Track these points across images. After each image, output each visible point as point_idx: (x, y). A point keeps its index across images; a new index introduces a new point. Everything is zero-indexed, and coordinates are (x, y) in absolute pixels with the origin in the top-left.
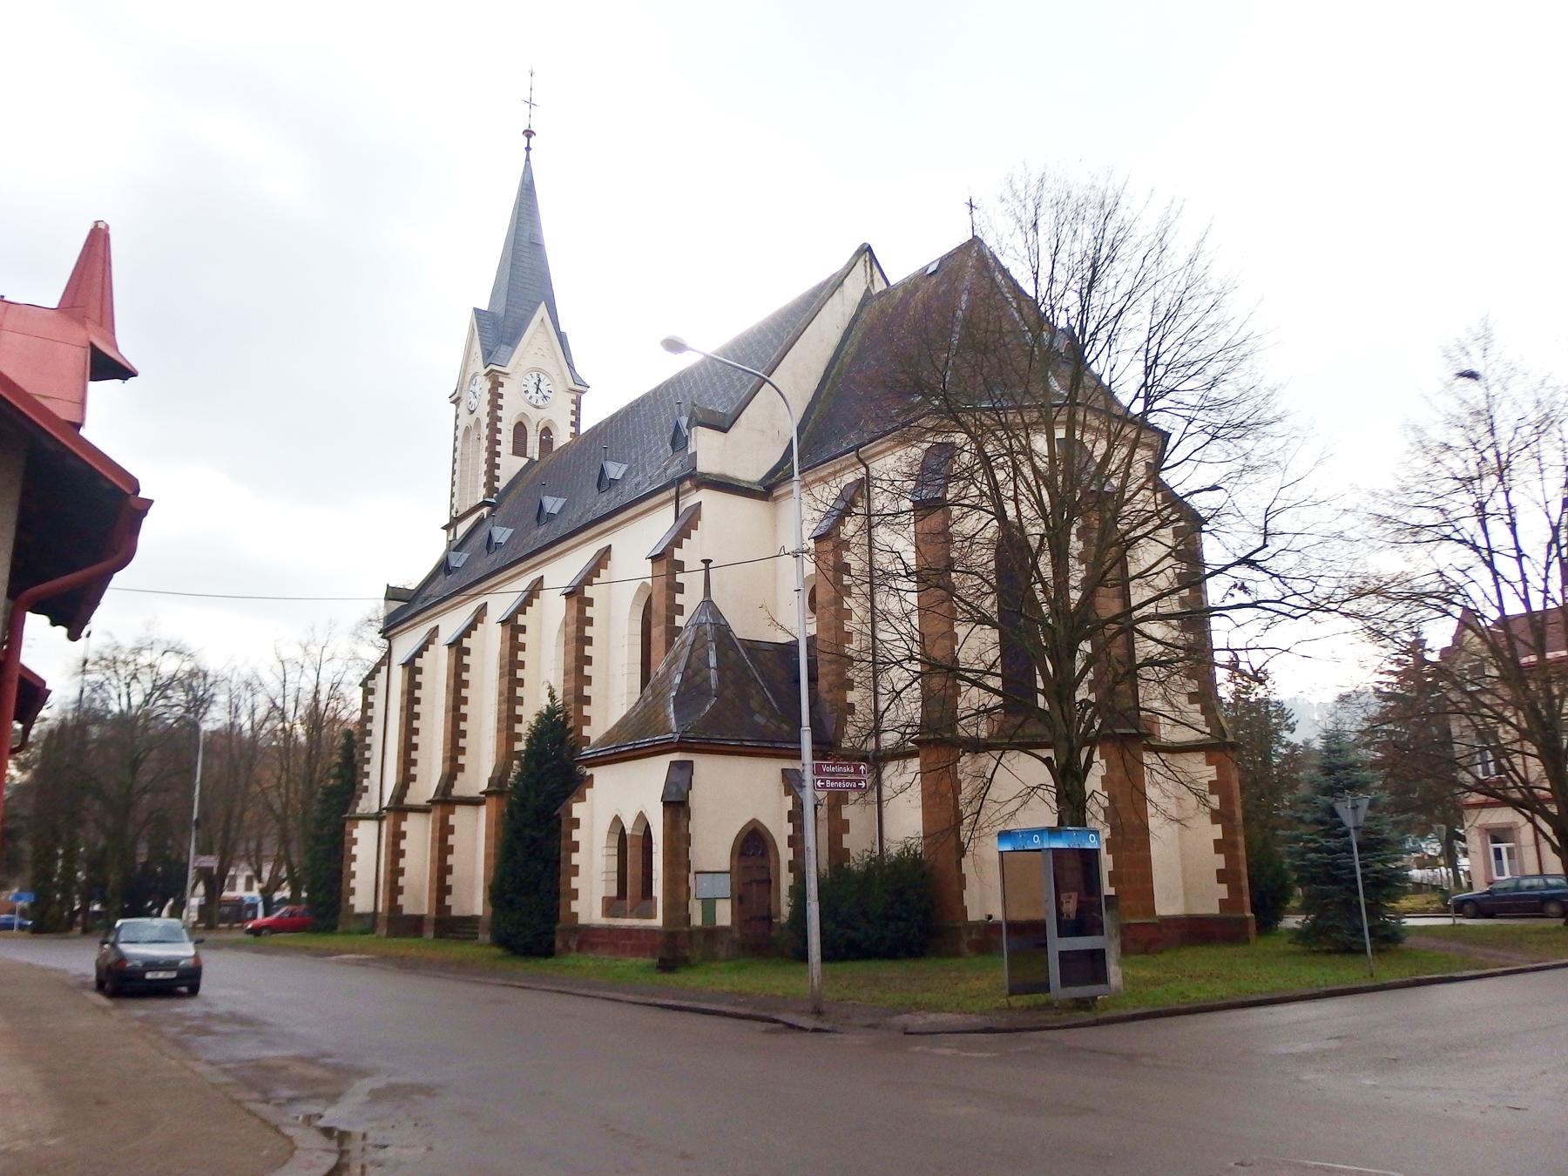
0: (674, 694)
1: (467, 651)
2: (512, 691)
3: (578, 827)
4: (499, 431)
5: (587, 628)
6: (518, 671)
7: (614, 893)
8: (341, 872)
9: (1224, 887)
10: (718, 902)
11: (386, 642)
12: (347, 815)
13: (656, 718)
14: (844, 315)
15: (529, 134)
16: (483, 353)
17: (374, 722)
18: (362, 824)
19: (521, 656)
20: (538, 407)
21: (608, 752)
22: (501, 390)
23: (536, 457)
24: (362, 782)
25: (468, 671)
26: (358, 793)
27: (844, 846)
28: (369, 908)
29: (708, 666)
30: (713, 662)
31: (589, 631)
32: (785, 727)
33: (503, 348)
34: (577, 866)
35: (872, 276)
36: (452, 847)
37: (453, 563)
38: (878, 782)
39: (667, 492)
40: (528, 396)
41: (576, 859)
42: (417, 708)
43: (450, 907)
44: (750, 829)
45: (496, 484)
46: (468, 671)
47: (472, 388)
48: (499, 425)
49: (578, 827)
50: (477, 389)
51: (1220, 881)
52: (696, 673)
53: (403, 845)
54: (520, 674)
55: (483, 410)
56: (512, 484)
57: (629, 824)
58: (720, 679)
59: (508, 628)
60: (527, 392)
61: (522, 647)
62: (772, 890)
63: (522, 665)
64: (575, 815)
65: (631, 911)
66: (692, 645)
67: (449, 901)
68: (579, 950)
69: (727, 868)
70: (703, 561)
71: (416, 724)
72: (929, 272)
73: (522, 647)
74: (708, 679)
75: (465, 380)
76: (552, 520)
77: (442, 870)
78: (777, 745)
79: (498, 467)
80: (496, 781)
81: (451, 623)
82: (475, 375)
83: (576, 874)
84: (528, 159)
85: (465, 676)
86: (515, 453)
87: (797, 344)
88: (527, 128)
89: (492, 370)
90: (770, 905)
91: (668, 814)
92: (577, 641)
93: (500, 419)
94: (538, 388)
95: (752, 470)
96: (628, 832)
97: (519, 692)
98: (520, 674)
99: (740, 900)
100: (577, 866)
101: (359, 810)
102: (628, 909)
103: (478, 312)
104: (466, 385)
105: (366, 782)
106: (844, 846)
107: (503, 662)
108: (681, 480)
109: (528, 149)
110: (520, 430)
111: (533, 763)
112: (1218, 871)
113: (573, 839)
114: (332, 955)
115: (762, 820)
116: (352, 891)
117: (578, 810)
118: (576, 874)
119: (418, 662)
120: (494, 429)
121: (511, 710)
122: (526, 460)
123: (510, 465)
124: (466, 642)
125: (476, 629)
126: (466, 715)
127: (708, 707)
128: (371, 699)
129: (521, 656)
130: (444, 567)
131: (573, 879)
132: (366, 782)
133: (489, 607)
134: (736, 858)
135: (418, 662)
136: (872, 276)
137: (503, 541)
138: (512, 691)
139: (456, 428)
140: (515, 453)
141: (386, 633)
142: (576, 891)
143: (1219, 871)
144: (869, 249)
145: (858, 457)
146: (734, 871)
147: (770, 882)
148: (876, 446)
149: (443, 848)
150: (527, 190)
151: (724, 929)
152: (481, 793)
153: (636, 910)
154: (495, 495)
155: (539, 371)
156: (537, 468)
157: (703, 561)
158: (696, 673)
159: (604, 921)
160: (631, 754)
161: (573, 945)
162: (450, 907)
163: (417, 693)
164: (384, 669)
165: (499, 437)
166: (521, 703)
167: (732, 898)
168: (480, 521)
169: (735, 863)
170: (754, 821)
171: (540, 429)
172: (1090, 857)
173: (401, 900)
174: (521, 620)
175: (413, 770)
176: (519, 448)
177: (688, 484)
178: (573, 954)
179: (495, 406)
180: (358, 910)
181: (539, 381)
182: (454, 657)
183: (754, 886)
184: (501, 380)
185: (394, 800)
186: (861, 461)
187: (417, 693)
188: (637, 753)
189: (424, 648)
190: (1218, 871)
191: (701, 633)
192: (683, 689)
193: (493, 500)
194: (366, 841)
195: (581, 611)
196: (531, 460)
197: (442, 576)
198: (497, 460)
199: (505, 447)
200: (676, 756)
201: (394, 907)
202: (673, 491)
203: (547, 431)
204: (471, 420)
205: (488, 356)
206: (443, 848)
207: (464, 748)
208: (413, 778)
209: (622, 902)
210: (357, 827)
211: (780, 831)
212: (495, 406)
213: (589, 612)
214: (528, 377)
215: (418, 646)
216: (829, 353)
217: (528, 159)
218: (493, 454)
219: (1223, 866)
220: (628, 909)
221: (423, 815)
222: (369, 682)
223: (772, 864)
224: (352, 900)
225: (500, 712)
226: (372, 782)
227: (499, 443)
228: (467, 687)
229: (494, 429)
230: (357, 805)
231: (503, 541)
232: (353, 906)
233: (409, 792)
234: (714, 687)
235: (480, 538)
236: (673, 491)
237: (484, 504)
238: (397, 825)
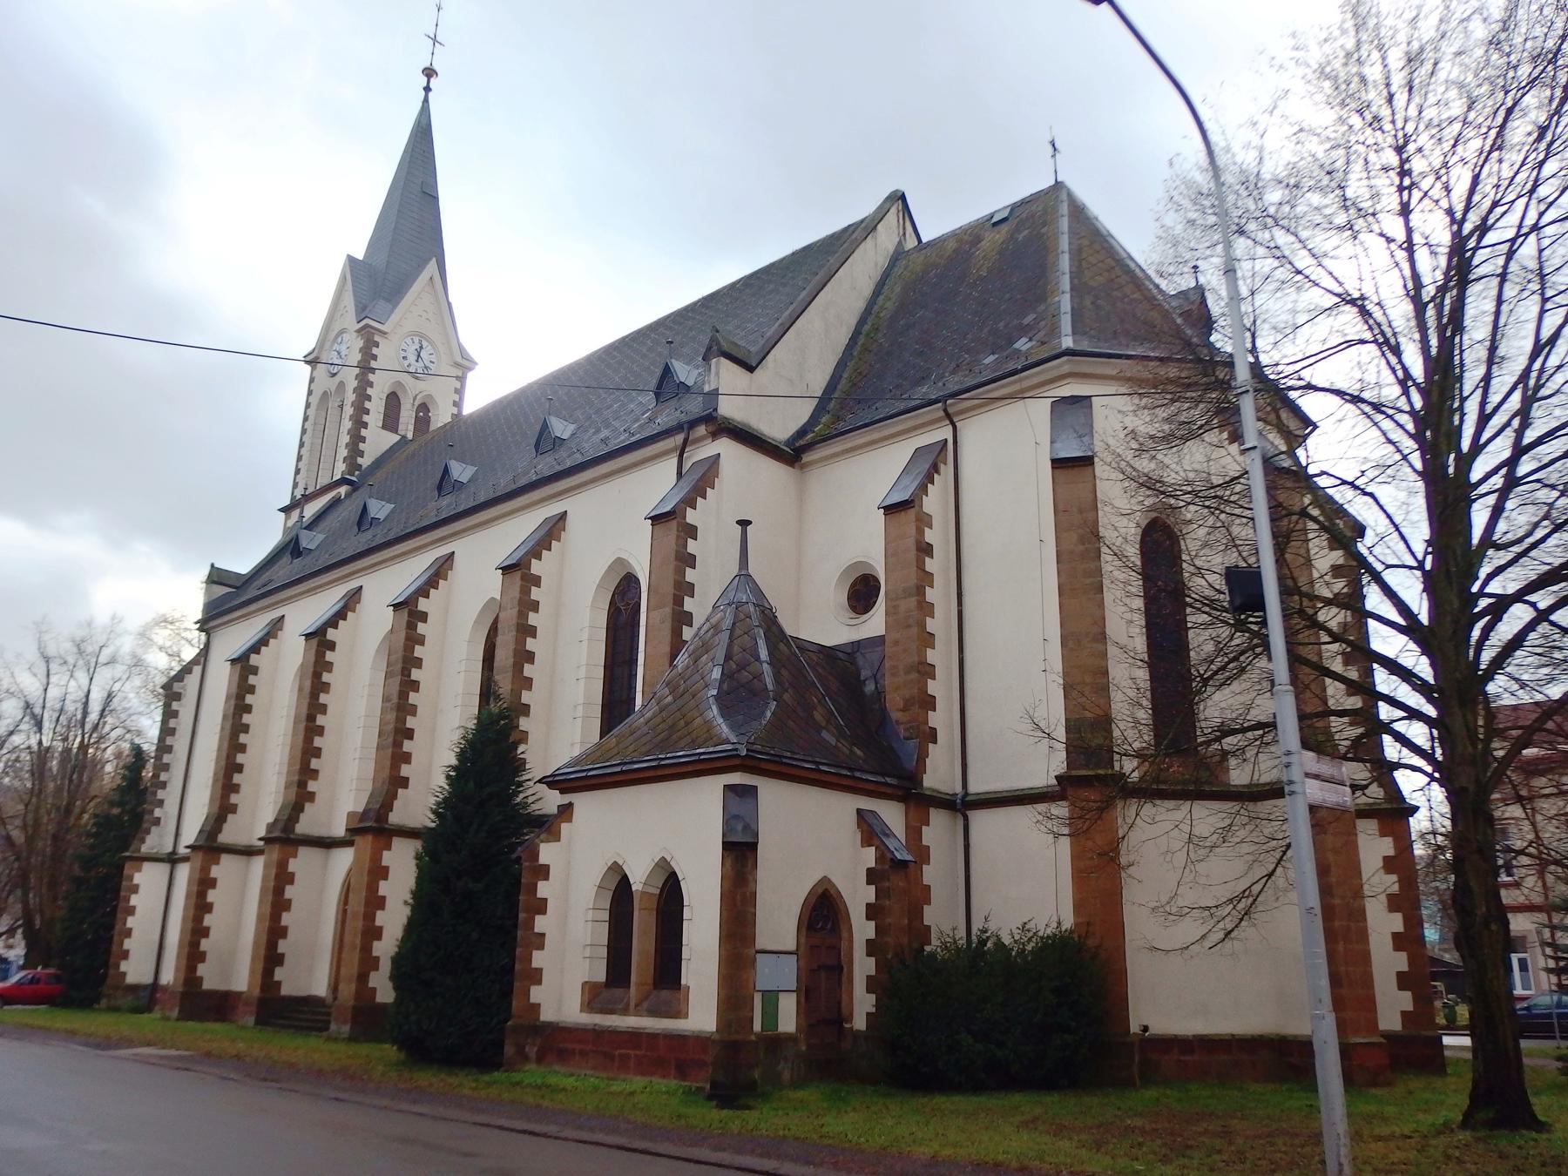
0: (715, 692)
1: (331, 646)
2: (403, 696)
3: (546, 878)
4: (369, 398)
5: (531, 615)
6: (413, 670)
7: (601, 976)
8: (112, 927)
9: (1408, 995)
10: (781, 995)
11: (203, 636)
12: (127, 854)
13: (687, 724)
14: (876, 264)
15: (429, 72)
16: (356, 306)
17: (177, 736)
18: (146, 866)
19: (419, 651)
21: (609, 771)
22: (375, 351)
23: (410, 436)
24: (152, 812)
25: (330, 671)
26: (145, 825)
28: (147, 979)
29: (758, 659)
30: (764, 654)
31: (533, 619)
32: (859, 752)
33: (382, 303)
34: (543, 935)
35: (904, 228)
36: (290, 901)
37: (304, 543)
39: (672, 439)
41: (541, 923)
42: (246, 718)
43: (279, 983)
44: (820, 891)
45: (360, 460)
46: (330, 671)
47: (336, 347)
48: (369, 391)
49: (546, 878)
50: (343, 348)
51: (1401, 987)
52: (742, 666)
53: (212, 896)
54: (415, 674)
55: (350, 378)
56: (378, 463)
57: (638, 877)
58: (777, 676)
59: (405, 614)
61: (421, 641)
62: (844, 979)
63: (418, 663)
64: (543, 860)
65: (637, 1005)
66: (732, 630)
67: (279, 974)
68: (540, 1059)
69: (792, 946)
70: (739, 522)
71: (243, 738)
72: (994, 220)
73: (421, 641)
74: (759, 677)
75: (329, 334)
76: (459, 489)
77: (196, 931)
78: (858, 774)
79: (363, 440)
80: (280, 825)
81: (305, 613)
82: (342, 332)
83: (541, 947)
84: (426, 100)
85: (326, 677)
86: (384, 427)
87: (829, 285)
88: (428, 65)
89: (367, 326)
90: (839, 1003)
91: (729, 863)
92: (517, 631)
93: (371, 385)
94: (419, 356)
95: (780, 425)
96: (636, 887)
97: (320, 720)
98: (415, 674)
99: (807, 994)
100: (543, 935)
101: (144, 849)
102: (632, 1004)
103: (351, 260)
104: (328, 345)
105: (157, 812)
107: (393, 658)
108: (693, 424)
109: (427, 89)
110: (393, 401)
111: (471, 784)
112: (1399, 974)
113: (539, 895)
114: (117, 1046)
115: (834, 880)
116: (125, 955)
117: (547, 853)
118: (541, 947)
119: (254, 659)
120: (362, 396)
121: (401, 720)
122: (397, 438)
123: (378, 441)
124: (331, 634)
125: (345, 619)
126: (323, 728)
127: (769, 714)
128: (175, 706)
129: (419, 651)
130: (290, 548)
131: (536, 954)
132: (157, 812)
133: (365, 592)
134: (804, 930)
135: (254, 659)
136: (904, 228)
137: (381, 516)
138: (403, 696)
139: (310, 393)
140: (384, 427)
141: (205, 625)
142: (539, 971)
143: (1400, 975)
144: (903, 197)
145: (945, 410)
146: (802, 949)
147: (842, 968)
148: (1003, 386)
149: (277, 902)
150: (422, 137)
151: (789, 1038)
152: (260, 839)
153: (645, 1005)
154: (357, 473)
155: (422, 336)
156: (412, 448)
157: (739, 522)
158: (742, 666)
160: (652, 773)
161: (532, 1051)
162: (279, 983)
163: (249, 699)
164: (197, 670)
165: (367, 405)
166: (414, 714)
167: (797, 991)
168: (336, 502)
169: (803, 940)
170: (825, 880)
171: (417, 403)
173: (201, 970)
174: (423, 604)
175: (234, 799)
176: (390, 423)
177: (701, 430)
178: (532, 1066)
179: (366, 368)
180: (130, 979)
181: (421, 347)
182: (313, 651)
183: (823, 975)
184: (377, 338)
185: (205, 835)
186: (948, 416)
187: (249, 699)
188: (660, 772)
189: (263, 642)
190: (1399, 974)
191: (742, 616)
192: (725, 686)
193: (354, 479)
194: (148, 884)
195: (526, 592)
196: (404, 437)
197: (286, 559)
198: (364, 432)
199: (375, 418)
200: (736, 778)
201: (190, 979)
202: (680, 438)
203: (424, 408)
204: (332, 384)
205: (362, 311)
206: (277, 902)
207: (316, 772)
208: (233, 809)
209: (618, 992)
210: (217, 863)
211: (857, 896)
212: (366, 368)
213: (535, 594)
214: (409, 341)
215: (256, 638)
216: (861, 305)
217: (426, 100)
218: (359, 424)
219: (1405, 968)
220: (632, 1004)
221: (244, 858)
222: (175, 684)
223: (844, 945)
224: (124, 966)
225: (382, 723)
226: (167, 812)
227: (367, 412)
228: (328, 692)
229: (362, 396)
230: (143, 841)
231: (381, 516)
232: (124, 974)
233: (226, 827)
234: (770, 687)
235: (349, 511)
236: (680, 438)
237: (343, 481)
238: (205, 870)
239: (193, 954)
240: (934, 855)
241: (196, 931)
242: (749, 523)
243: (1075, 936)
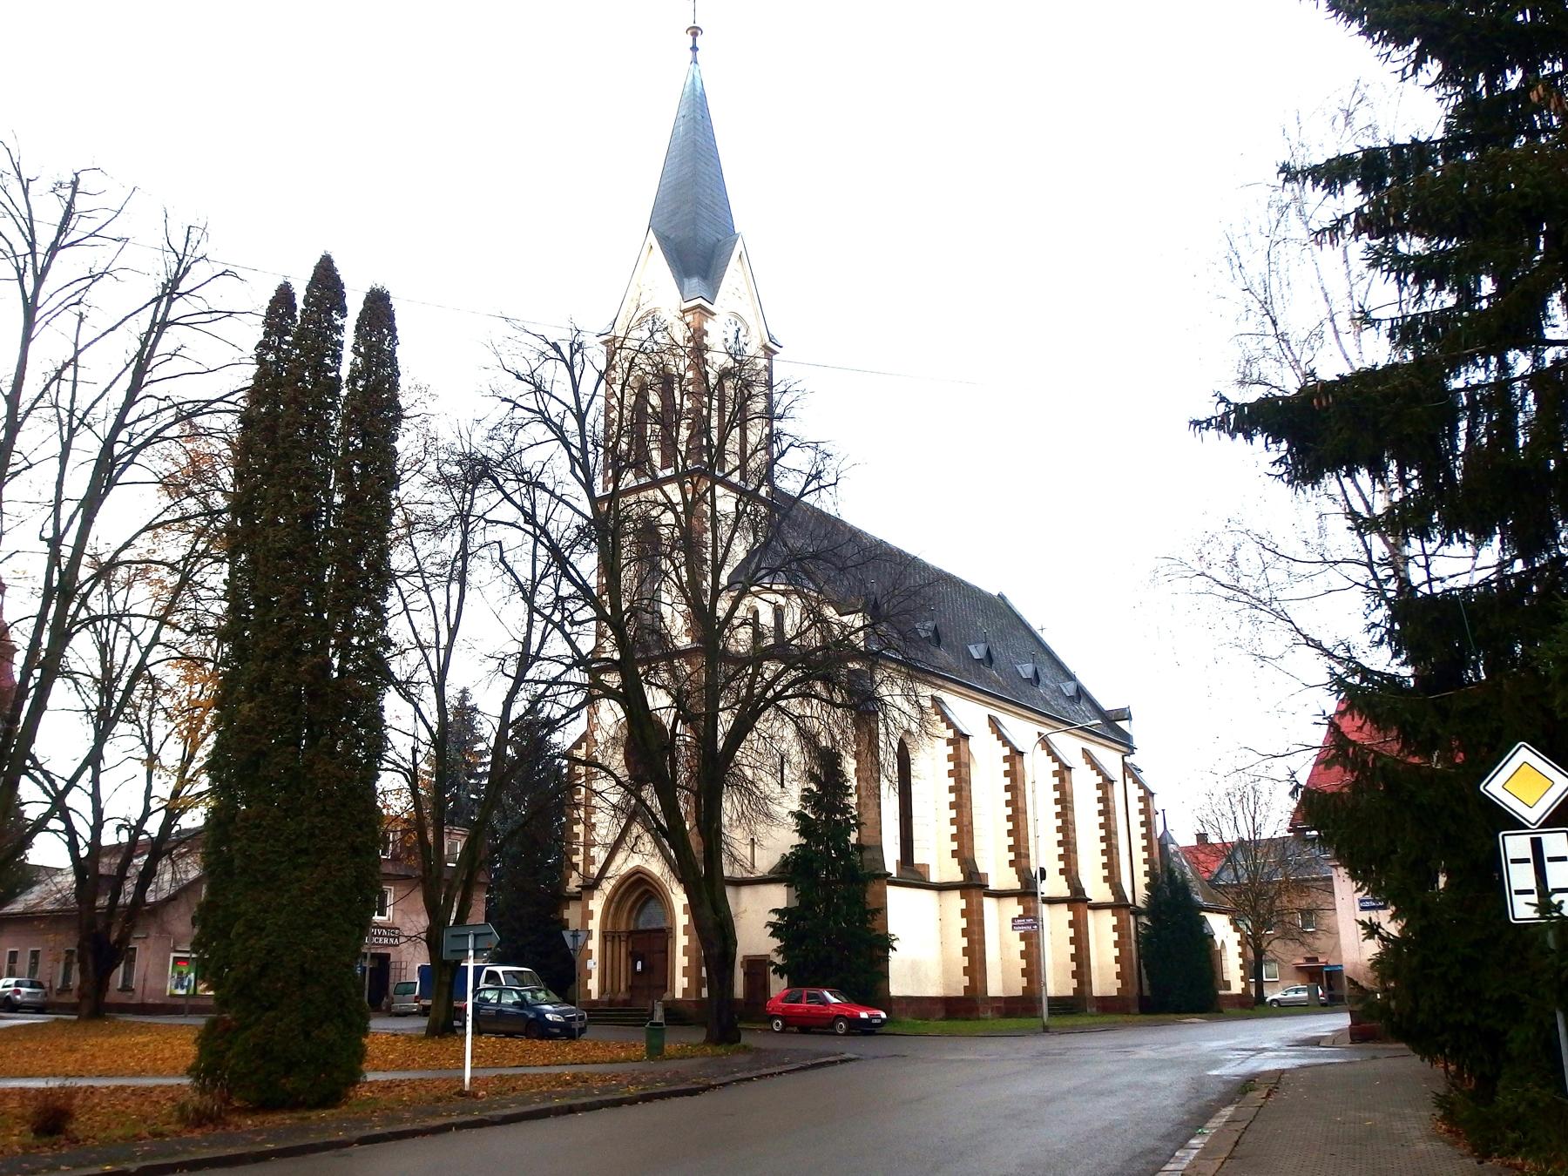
15: (695, 31)
109: (694, 49)
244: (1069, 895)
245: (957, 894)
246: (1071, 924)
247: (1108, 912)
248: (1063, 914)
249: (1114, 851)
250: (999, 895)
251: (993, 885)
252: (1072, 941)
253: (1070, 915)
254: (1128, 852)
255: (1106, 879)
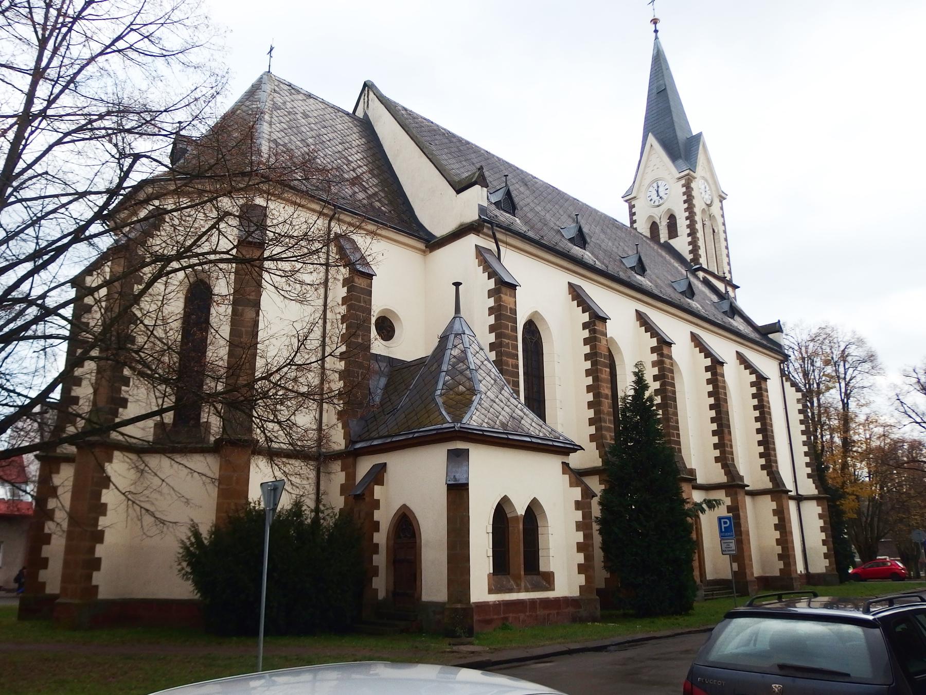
15: (655, 21)
20: (658, 206)
27: (375, 498)
38: (379, 380)
40: (653, 202)
53: (776, 520)
60: (651, 200)
77: (785, 541)
84: (656, 38)
88: (652, 18)
106: (375, 498)
109: (656, 31)
150: (659, 63)
159: (619, 397)
170: (404, 507)
172: (360, 302)
217: (656, 38)
239: (786, 555)
240: (338, 490)
241: (785, 541)
242: (461, 284)
243: (687, 506)
244: (726, 481)
245: (768, 497)
246: (775, 512)
247: (768, 498)
248: (768, 505)
249: (726, 431)
250: (754, 494)
251: (700, 480)
252: (777, 527)
253: (774, 505)
254: (787, 441)
255: (717, 460)
